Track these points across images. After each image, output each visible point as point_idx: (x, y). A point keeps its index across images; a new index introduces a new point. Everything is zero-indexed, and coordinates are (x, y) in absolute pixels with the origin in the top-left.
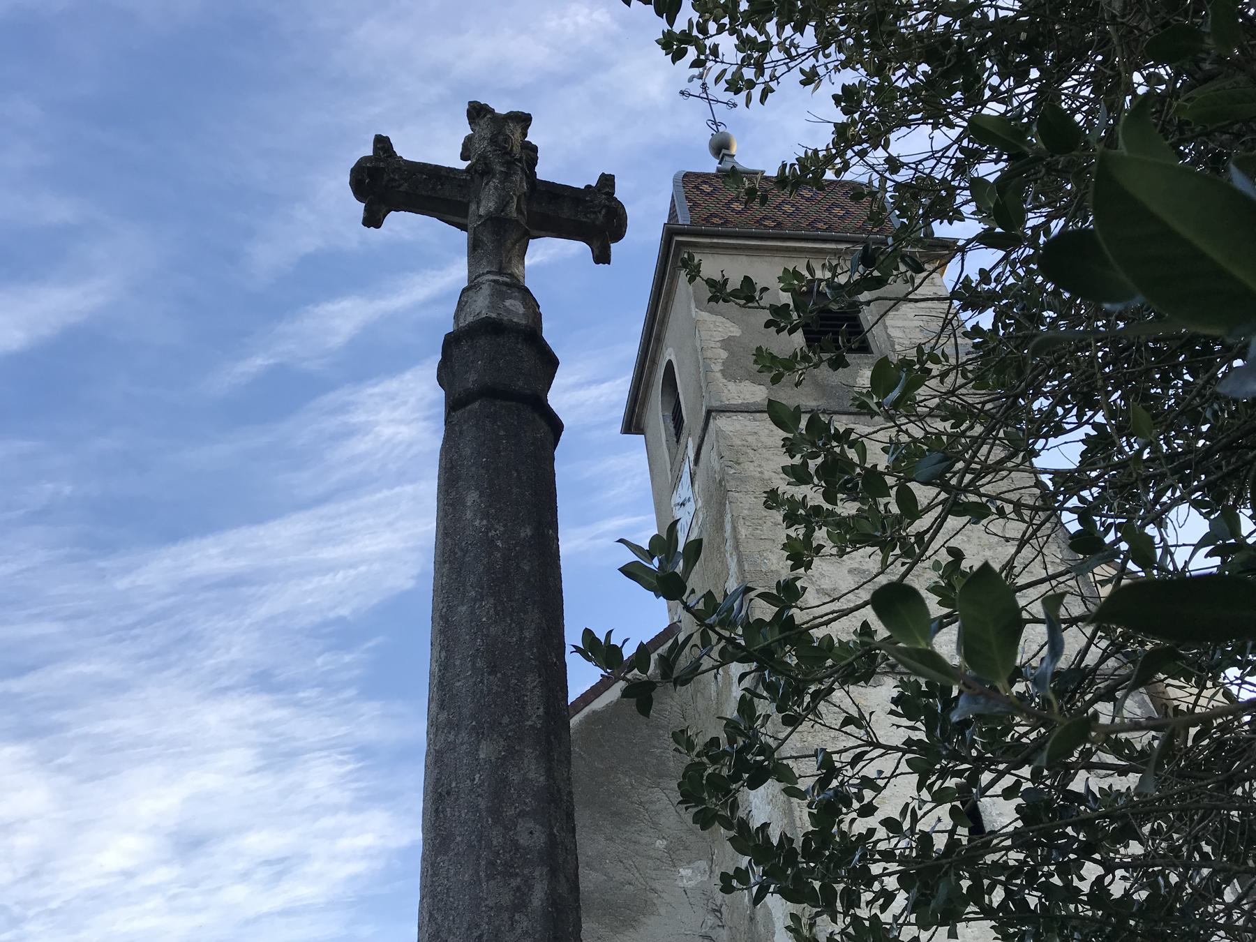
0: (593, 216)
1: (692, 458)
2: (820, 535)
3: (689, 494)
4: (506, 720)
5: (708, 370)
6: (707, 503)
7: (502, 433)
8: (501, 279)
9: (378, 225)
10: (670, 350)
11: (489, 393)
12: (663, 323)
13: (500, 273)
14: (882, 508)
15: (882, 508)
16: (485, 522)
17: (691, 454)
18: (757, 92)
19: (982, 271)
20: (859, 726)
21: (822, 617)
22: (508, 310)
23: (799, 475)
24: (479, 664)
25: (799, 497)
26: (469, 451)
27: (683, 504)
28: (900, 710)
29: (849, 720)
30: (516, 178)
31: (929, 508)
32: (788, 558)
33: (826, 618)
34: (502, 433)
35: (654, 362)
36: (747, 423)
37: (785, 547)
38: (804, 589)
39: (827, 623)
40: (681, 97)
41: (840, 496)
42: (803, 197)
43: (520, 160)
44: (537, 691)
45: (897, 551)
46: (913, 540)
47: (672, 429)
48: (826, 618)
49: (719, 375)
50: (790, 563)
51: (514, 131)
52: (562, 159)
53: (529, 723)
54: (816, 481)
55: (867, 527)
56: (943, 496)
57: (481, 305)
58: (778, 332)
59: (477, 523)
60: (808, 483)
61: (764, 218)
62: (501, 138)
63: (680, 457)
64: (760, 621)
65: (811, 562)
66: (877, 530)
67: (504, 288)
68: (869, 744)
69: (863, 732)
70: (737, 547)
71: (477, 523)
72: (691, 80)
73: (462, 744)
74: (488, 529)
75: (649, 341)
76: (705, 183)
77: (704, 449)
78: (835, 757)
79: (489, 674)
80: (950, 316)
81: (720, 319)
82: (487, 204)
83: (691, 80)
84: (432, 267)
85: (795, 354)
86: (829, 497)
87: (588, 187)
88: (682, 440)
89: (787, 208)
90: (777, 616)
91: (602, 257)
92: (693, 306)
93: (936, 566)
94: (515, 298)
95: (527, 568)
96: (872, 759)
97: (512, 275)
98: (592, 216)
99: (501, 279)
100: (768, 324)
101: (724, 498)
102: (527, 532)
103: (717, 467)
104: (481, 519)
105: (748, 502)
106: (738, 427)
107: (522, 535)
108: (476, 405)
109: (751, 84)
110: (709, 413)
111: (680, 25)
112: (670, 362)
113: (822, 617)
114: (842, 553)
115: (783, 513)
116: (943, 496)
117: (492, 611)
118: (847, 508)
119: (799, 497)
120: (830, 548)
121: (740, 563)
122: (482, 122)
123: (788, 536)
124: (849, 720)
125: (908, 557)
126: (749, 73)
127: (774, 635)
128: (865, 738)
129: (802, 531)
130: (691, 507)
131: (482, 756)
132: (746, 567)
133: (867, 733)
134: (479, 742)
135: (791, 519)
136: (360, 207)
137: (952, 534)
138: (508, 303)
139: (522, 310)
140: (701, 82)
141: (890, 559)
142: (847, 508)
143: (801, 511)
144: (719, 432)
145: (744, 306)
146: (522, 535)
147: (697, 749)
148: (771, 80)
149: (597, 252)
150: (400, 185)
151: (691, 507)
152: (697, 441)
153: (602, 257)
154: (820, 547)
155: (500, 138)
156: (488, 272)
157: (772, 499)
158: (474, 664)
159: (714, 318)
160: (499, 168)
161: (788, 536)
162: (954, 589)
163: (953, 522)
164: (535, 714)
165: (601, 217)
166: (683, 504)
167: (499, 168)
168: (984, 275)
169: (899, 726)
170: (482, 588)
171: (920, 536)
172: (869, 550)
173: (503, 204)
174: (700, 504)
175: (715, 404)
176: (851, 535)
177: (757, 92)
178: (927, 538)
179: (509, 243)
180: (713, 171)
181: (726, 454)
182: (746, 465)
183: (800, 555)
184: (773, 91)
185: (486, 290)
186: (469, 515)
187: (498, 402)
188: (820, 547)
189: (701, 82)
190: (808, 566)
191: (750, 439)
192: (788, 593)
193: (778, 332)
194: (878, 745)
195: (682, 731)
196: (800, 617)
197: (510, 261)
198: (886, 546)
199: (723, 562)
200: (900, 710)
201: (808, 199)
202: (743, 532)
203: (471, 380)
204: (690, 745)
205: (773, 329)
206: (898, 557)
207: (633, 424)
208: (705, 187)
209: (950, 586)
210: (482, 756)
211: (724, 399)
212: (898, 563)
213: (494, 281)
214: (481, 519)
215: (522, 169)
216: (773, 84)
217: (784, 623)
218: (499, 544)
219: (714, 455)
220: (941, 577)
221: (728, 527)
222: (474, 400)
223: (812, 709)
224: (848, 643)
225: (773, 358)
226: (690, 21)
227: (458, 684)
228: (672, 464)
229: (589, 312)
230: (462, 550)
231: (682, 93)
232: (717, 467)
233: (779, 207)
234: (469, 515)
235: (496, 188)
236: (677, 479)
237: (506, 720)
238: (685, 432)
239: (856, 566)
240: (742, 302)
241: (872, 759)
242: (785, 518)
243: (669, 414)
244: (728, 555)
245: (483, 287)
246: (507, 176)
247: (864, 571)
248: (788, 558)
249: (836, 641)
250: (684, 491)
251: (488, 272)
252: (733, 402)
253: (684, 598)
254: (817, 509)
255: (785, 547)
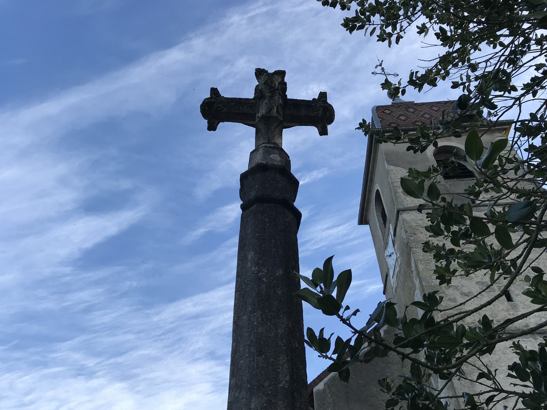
0: (316, 113)
1: (392, 233)
2: (454, 265)
3: (393, 251)
4: (266, 384)
5: (396, 192)
6: (402, 254)
7: (267, 220)
8: (268, 145)
9: (214, 129)
10: (377, 185)
11: (260, 200)
12: (373, 173)
13: (269, 143)
14: (489, 248)
15: (489, 248)
16: (257, 268)
17: (392, 232)
18: (394, 38)
19: (531, 114)
20: (489, 379)
21: (453, 316)
22: (271, 159)
23: (435, 231)
24: (252, 350)
25: (441, 244)
26: (250, 231)
27: (390, 256)
28: (514, 374)
29: (482, 375)
30: (276, 98)
31: (518, 245)
32: (437, 278)
33: (455, 317)
34: (267, 220)
35: (370, 191)
36: (418, 215)
37: (435, 272)
38: (442, 298)
39: (461, 318)
40: (373, 75)
41: (461, 242)
42: (433, 110)
43: (278, 89)
44: (285, 366)
45: (501, 271)
46: (509, 264)
47: (382, 221)
48: (455, 317)
49: (401, 194)
50: (438, 281)
51: (278, 79)
52: (301, 89)
53: (281, 385)
54: (446, 233)
55: (479, 258)
56: (526, 236)
57: (259, 159)
58: (415, 152)
59: (253, 269)
60: (441, 235)
61: (416, 121)
62: (269, 81)
63: (387, 233)
64: (414, 320)
65: (450, 280)
66: (485, 259)
67: (270, 149)
68: (495, 390)
69: (491, 382)
70: (418, 274)
71: (253, 269)
72: (376, 67)
73: (242, 398)
74: (259, 272)
75: (367, 183)
76: (386, 109)
77: (398, 229)
78: (476, 398)
79: (258, 356)
80: (516, 139)
81: (399, 168)
82: (262, 111)
83: (376, 67)
84: (239, 144)
85: (430, 169)
86: (455, 242)
87: (314, 99)
88: (387, 226)
89: (426, 116)
90: (424, 316)
91: (323, 132)
92: (386, 164)
93: (527, 278)
94: (275, 154)
95: (280, 293)
96: (499, 401)
97: (275, 143)
98: (319, 114)
99: (268, 145)
100: (408, 149)
101: (410, 251)
102: (280, 272)
103: (405, 237)
104: (255, 267)
105: (418, 251)
106: (413, 217)
107: (277, 274)
108: (254, 207)
109: (390, 35)
110: (398, 212)
111: (351, 14)
112: (378, 191)
113: (453, 316)
114: (467, 274)
115: (432, 254)
116: (526, 236)
117: (259, 319)
118: (470, 248)
119: (441, 244)
120: (460, 271)
121: (421, 282)
122: (262, 77)
123: (436, 266)
124: (482, 375)
125: (507, 274)
126: (389, 30)
127: (421, 330)
128: (493, 386)
129: (444, 263)
130: (394, 257)
131: (253, 407)
132: (424, 284)
133: (495, 383)
134: (251, 397)
135: (438, 257)
136: (205, 122)
137: (531, 261)
138: (272, 156)
139: (279, 159)
140: (381, 67)
141: (496, 276)
142: (470, 248)
143: (443, 252)
144: (404, 220)
145: (395, 143)
146: (277, 274)
147: (392, 391)
148: (401, 31)
149: (320, 130)
150: (223, 109)
151: (394, 257)
152: (394, 225)
153: (323, 132)
154: (455, 271)
155: (271, 83)
156: (263, 143)
157: (427, 247)
158: (249, 350)
159: (396, 168)
160: (268, 94)
161: (436, 266)
162: (541, 292)
163: (535, 252)
164: (284, 380)
165: (320, 112)
166: (390, 256)
167: (268, 94)
168: (533, 116)
169: (515, 385)
170: (255, 305)
171: (513, 261)
172: (485, 271)
173: (270, 110)
174: (398, 255)
175: (401, 207)
176: (472, 264)
177: (394, 38)
178: (519, 262)
179: (273, 128)
180: (391, 104)
181: (409, 230)
182: (419, 235)
183: (444, 276)
184: (402, 37)
185: (261, 151)
186: (249, 265)
187: (265, 205)
188: (455, 271)
189: (381, 67)
190: (449, 282)
191: (420, 222)
192: (431, 301)
193: (415, 152)
194: (502, 391)
195: (384, 380)
196: (438, 317)
197: (274, 136)
198: (493, 268)
199: (412, 282)
200: (514, 374)
201: (436, 111)
202: (421, 267)
203: (252, 194)
204: (389, 388)
205: (412, 151)
206: (501, 275)
207: (363, 220)
208: (387, 111)
209: (538, 290)
210: (253, 407)
211: (405, 204)
212: (502, 278)
213: (265, 146)
214: (255, 267)
215: (279, 93)
216: (402, 34)
217: (428, 321)
218: (264, 280)
219: (403, 231)
220: (531, 285)
221: (413, 265)
222: (253, 205)
223: (458, 366)
224: (475, 328)
225: (418, 172)
226: (356, 10)
227: (241, 362)
228: (383, 237)
229: (326, 163)
230: (245, 284)
231: (373, 73)
232: (405, 237)
233: (422, 116)
234: (249, 265)
235: (266, 104)
236: (387, 244)
237: (266, 384)
238: (388, 222)
239: (480, 280)
240: (395, 141)
241: (499, 401)
242: (435, 256)
243: (380, 214)
244: (414, 279)
245: (260, 150)
246: (271, 97)
247: (484, 283)
248: (437, 278)
249: (467, 328)
250: (390, 249)
251: (263, 143)
252: (409, 206)
253: (340, 313)
254: (452, 251)
255: (435, 272)
